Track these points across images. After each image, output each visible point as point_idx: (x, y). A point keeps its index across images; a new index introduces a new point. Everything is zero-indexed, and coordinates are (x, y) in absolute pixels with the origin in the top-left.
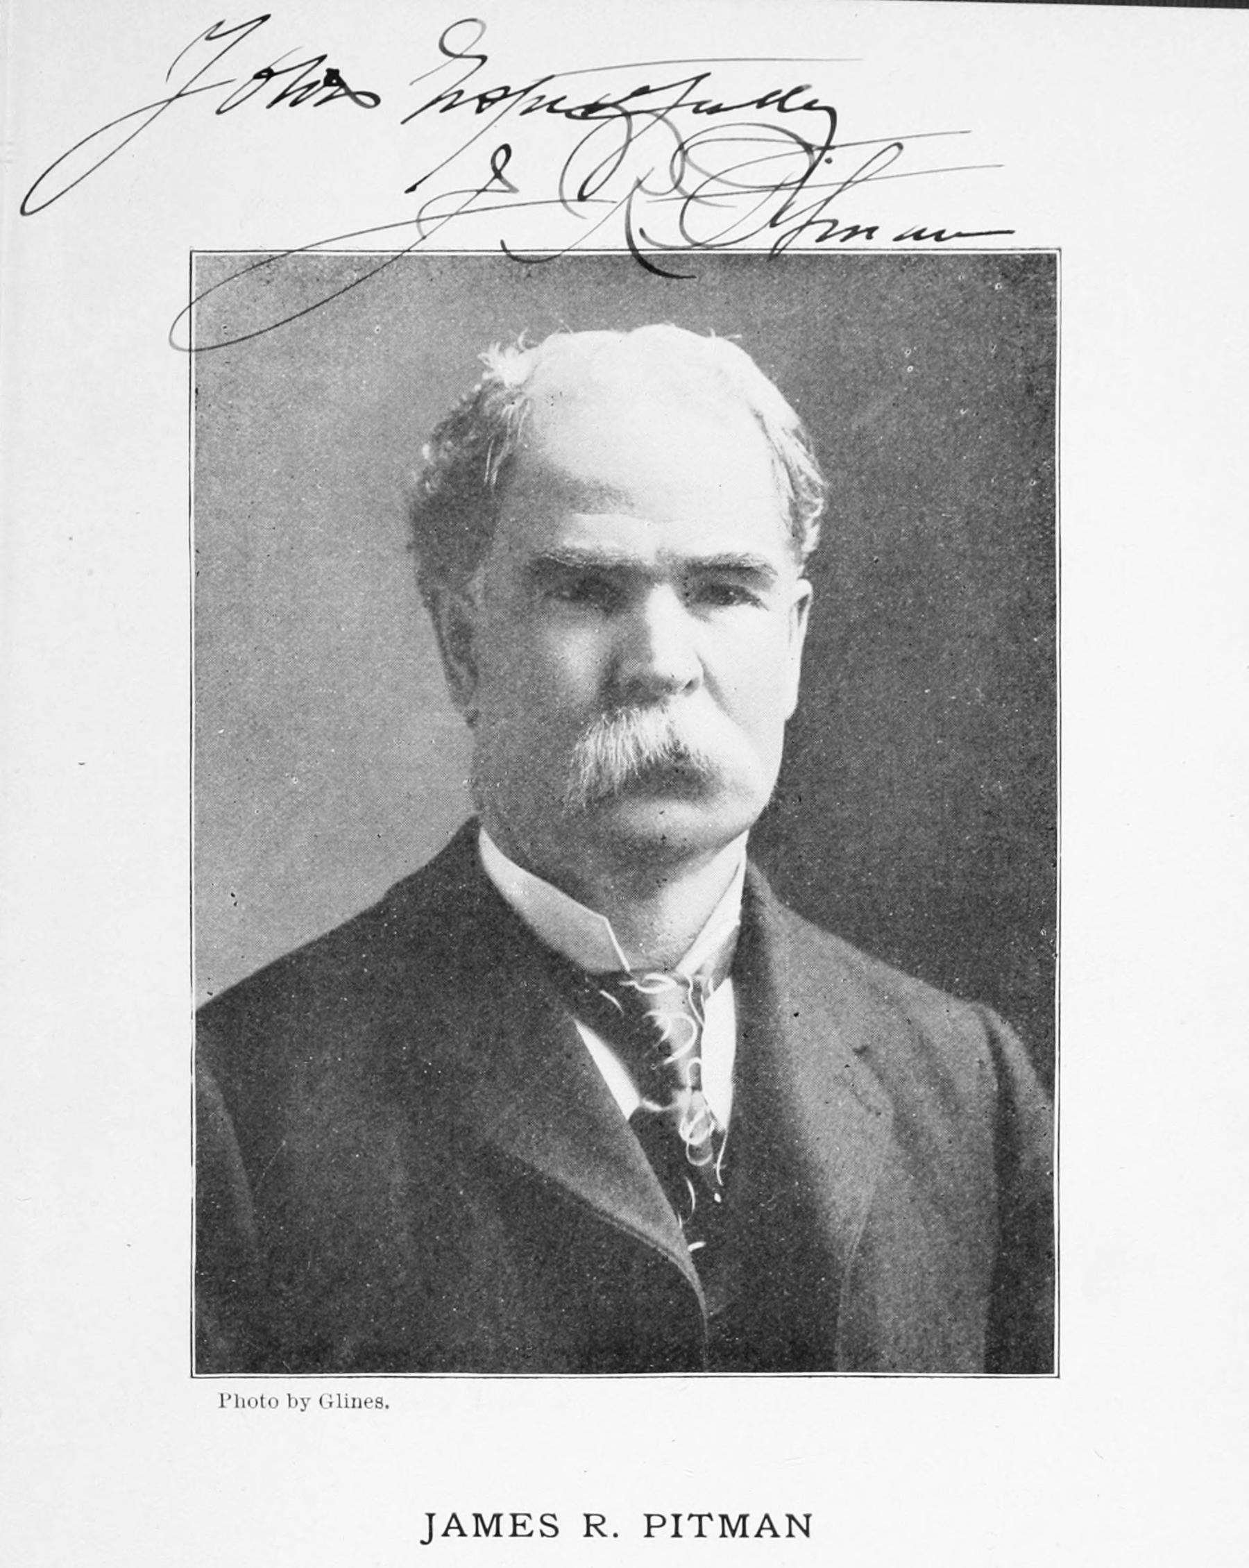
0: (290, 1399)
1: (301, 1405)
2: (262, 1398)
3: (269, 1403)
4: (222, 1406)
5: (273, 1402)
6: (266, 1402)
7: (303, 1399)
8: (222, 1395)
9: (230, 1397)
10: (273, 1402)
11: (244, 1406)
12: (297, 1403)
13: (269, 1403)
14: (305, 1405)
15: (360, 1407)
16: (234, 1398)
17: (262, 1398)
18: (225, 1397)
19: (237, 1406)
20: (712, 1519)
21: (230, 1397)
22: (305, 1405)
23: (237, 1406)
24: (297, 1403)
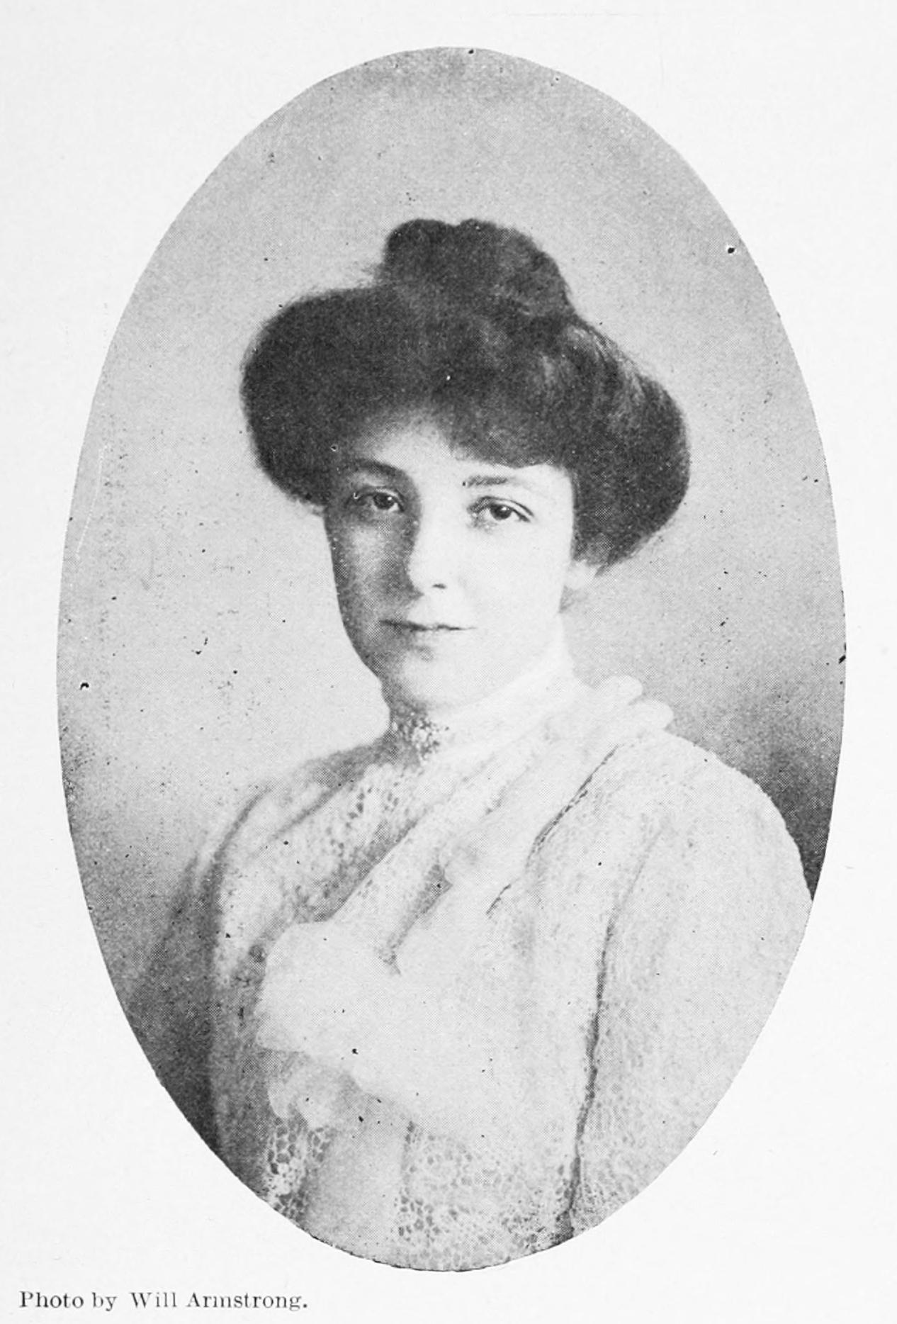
0: (39, 1298)
1: (106, 1305)
2: (65, 1297)
3: (74, 1303)
4: (24, 1305)
5: (78, 1302)
6: (69, 1301)
7: (108, 1298)
8: (23, 1294)
9: (32, 1295)
10: (78, 1302)
11: (46, 1306)
12: (102, 1301)
13: (74, 1303)
14: (111, 1305)
15: (278, 1299)
16: (35, 1296)
17: (65, 1297)
18: (27, 1296)
19: (39, 1305)
20: (300, 1297)
21: (32, 1295)
22: (111, 1305)
23: (39, 1305)
24: (102, 1301)
